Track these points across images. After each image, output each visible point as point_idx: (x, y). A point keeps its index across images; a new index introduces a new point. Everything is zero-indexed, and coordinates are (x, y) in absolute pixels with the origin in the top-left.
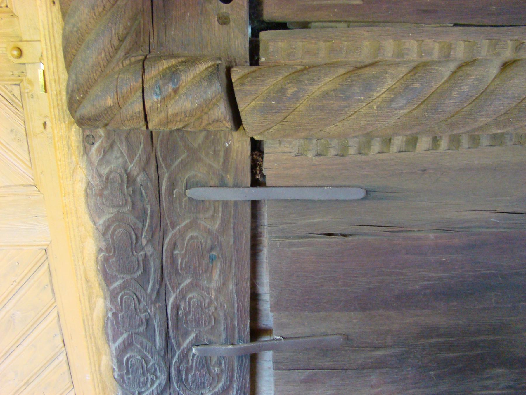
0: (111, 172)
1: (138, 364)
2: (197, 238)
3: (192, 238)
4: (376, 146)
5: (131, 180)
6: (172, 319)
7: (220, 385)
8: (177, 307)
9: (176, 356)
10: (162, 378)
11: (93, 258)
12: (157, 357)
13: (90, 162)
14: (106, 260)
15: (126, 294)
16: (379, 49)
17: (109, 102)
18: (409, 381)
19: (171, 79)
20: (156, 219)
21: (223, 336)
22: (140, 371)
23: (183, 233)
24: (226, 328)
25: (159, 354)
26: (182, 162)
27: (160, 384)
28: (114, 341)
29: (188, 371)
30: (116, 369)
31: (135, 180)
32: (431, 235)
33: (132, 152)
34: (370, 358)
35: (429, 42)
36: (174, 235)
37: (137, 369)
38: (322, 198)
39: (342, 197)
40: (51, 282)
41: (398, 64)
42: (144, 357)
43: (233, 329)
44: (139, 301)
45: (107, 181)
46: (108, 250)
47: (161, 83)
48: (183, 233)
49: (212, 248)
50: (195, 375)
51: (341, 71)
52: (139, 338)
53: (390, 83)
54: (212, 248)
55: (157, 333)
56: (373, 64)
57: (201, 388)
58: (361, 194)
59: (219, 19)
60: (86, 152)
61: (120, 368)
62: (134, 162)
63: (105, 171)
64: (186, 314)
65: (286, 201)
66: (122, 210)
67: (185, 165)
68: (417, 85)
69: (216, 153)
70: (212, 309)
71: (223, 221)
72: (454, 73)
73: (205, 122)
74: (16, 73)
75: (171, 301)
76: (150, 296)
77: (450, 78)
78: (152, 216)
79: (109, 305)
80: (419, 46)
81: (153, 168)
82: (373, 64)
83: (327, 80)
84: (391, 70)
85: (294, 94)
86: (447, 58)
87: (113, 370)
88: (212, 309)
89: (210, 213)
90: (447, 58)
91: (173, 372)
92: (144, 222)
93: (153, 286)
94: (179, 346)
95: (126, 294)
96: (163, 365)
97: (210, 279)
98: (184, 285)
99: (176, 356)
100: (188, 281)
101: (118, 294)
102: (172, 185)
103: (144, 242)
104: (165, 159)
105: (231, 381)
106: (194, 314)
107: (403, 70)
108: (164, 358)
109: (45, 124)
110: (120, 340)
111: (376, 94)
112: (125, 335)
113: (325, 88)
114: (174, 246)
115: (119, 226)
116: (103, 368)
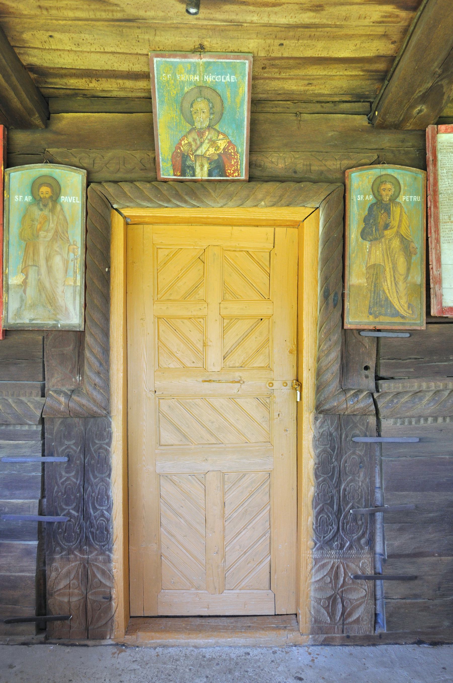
0: (323, 431)
1: (325, 520)
2: (355, 458)
3: (353, 458)
4: (422, 421)
5: (331, 435)
6: (342, 496)
7: (361, 531)
8: (345, 490)
9: (343, 515)
10: (335, 527)
11: (312, 467)
12: (334, 516)
13: (316, 427)
14: (318, 468)
15: (324, 484)
16: (420, 386)
17: (335, 404)
18: (447, 531)
19: (356, 397)
20: (339, 450)
21: (364, 504)
22: (325, 525)
23: (349, 457)
24: (365, 500)
25: (335, 514)
26: (350, 428)
27: (334, 531)
28: (315, 508)
29: (347, 523)
30: (315, 524)
31: (332, 434)
32: (447, 457)
33: (332, 424)
34: (427, 517)
35: (439, 383)
36: (346, 457)
37: (324, 523)
38: (403, 441)
39: (410, 441)
40: (269, 490)
41: (429, 391)
42: (328, 516)
43: (368, 500)
44: (329, 487)
45: (322, 435)
46: (319, 464)
47: (353, 398)
48: (349, 457)
49: (361, 463)
50: (350, 525)
51: (410, 394)
52: (327, 506)
53: (427, 398)
54: (361, 463)
55: (335, 503)
56: (420, 392)
57: (353, 534)
58: (417, 440)
59: (365, 376)
60: (315, 423)
61: (316, 523)
62: (334, 426)
63: (321, 431)
64: (349, 493)
65: (389, 442)
66: (326, 446)
67: (352, 429)
68: (437, 398)
69: (363, 424)
70: (360, 490)
71: (366, 451)
72: (449, 394)
73: (367, 411)
74: (269, 393)
75: (343, 487)
76: (334, 485)
77: (447, 396)
78: (338, 449)
79: (316, 490)
80: (435, 385)
81: (340, 429)
82: (420, 392)
83: (406, 397)
84: (427, 393)
85: (397, 402)
86: (446, 388)
87: (313, 524)
88: (360, 490)
89: (360, 448)
90: (446, 388)
91: (341, 524)
92: (334, 452)
93: (336, 480)
94: (344, 510)
95: (324, 484)
96: (336, 521)
97: (359, 477)
98: (348, 479)
99: (343, 515)
100: (350, 477)
101: (320, 484)
102: (347, 436)
103: (334, 460)
104: (344, 426)
105: (367, 529)
106: (352, 494)
107: (431, 394)
108: (337, 516)
109: (279, 415)
110: (318, 508)
111: (423, 402)
112: (321, 505)
113: (406, 400)
114: (346, 462)
115: (324, 453)
116: (309, 523)
